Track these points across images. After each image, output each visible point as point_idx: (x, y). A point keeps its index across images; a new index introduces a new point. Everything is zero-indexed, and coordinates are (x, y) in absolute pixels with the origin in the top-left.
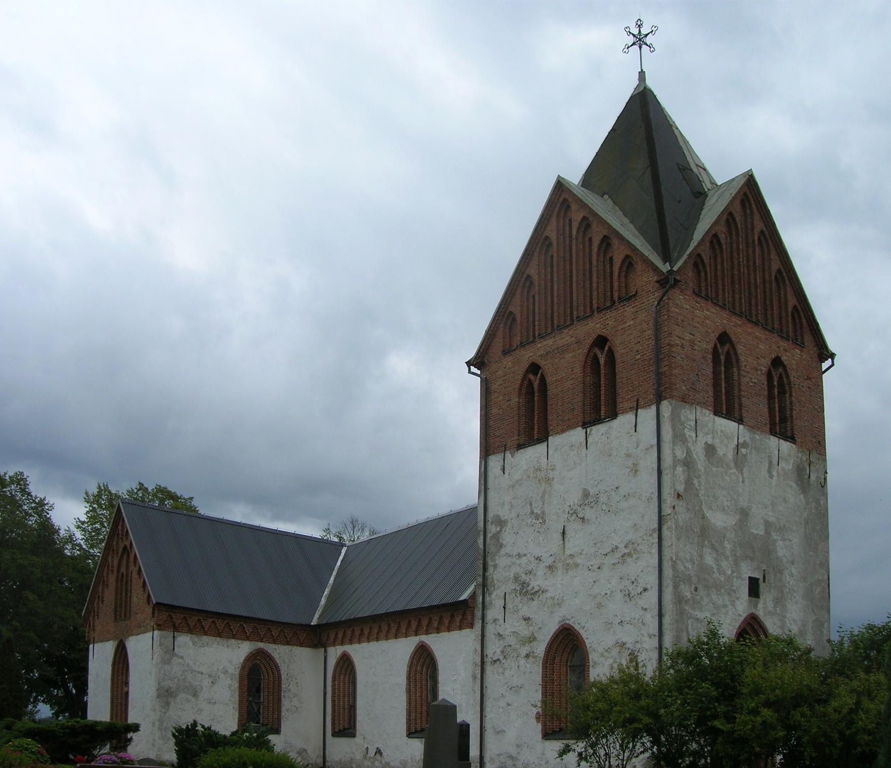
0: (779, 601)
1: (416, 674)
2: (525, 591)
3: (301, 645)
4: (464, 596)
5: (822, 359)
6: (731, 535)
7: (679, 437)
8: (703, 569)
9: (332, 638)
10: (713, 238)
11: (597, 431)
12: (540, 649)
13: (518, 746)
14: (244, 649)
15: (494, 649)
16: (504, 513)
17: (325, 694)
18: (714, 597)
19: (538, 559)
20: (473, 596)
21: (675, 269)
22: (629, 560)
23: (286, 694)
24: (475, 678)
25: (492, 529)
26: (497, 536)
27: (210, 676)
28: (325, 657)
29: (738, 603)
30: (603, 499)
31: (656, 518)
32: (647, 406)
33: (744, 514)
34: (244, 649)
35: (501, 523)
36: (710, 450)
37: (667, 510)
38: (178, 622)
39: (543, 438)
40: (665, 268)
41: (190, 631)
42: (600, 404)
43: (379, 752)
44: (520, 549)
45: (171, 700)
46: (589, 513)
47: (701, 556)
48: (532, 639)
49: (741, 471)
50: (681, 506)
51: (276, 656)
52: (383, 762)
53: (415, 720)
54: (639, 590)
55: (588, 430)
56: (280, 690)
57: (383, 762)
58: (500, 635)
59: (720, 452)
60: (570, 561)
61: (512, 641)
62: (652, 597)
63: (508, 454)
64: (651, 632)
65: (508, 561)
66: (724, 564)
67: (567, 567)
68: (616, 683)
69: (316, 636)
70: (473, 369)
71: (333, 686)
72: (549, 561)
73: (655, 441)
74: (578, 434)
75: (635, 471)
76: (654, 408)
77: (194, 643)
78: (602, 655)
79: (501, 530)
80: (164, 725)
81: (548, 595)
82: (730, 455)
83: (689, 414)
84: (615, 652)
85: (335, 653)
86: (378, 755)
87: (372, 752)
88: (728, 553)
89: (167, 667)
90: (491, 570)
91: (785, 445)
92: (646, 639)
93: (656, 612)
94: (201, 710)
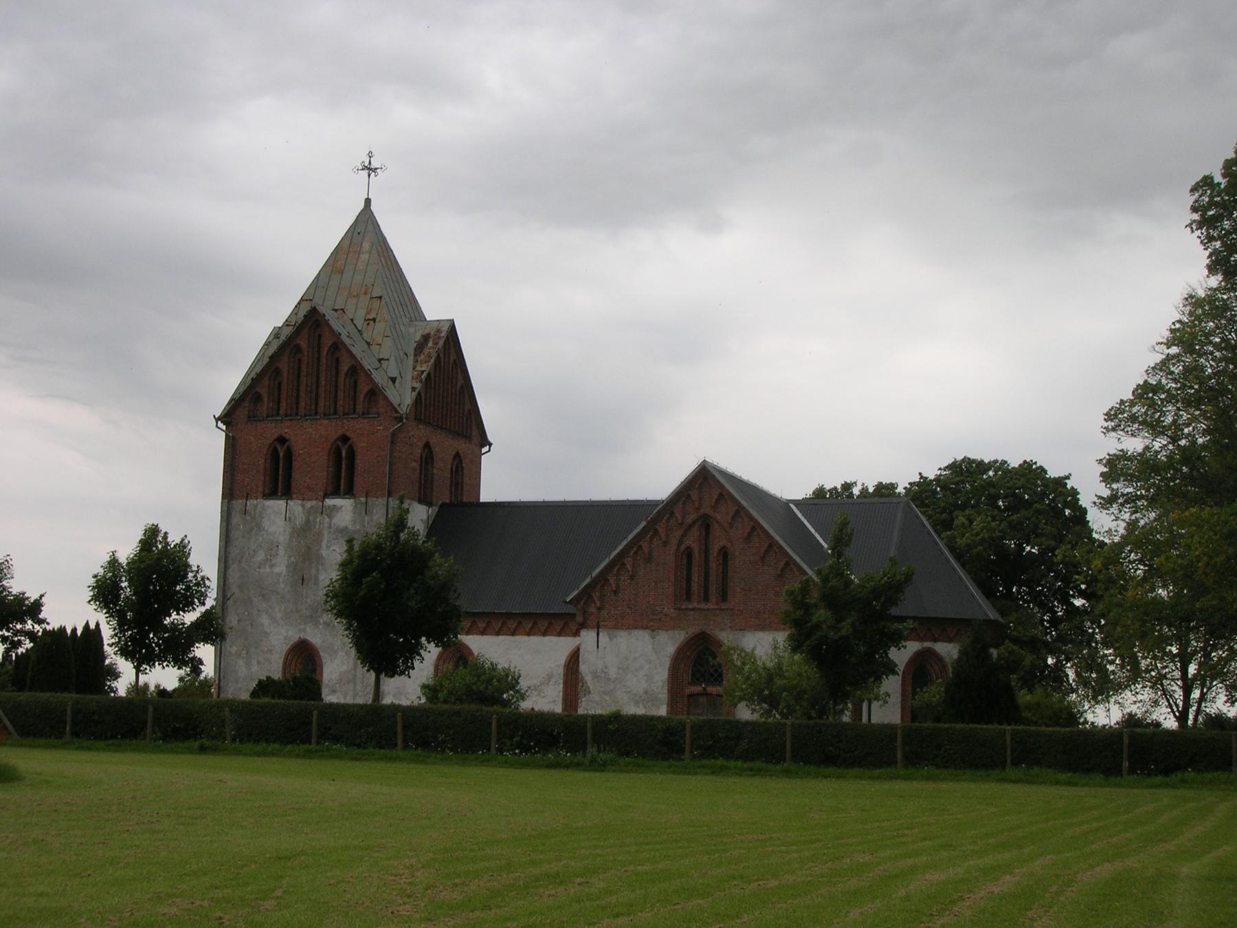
5: (483, 446)
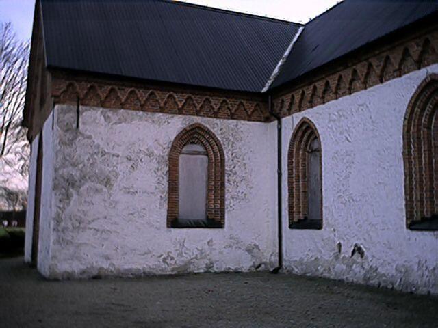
1: (419, 130)
3: (249, 118)
9: (287, 104)
14: (176, 124)
17: (280, 175)
23: (231, 178)
27: (129, 159)
28: (279, 131)
34: (176, 124)
38: (82, 94)
41: (102, 104)
43: (358, 250)
45: (72, 191)
51: (216, 132)
52: (366, 267)
53: (422, 201)
56: (223, 173)
57: (366, 267)
69: (267, 106)
71: (290, 164)
77: (106, 118)
80: (63, 224)
85: (290, 123)
86: (356, 254)
87: (347, 251)
89: (68, 150)
94: (116, 202)
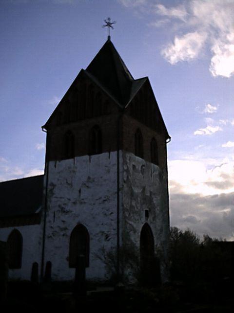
0: (154, 219)
2: (63, 211)
4: (37, 212)
6: (140, 195)
7: (125, 163)
8: (132, 207)
10: (136, 98)
11: (94, 157)
12: (69, 233)
13: (59, 270)
15: (49, 232)
16: (55, 182)
18: (135, 216)
19: (69, 200)
20: (41, 212)
21: (126, 107)
22: (106, 202)
24: (40, 243)
25: (50, 187)
26: (51, 190)
29: (142, 219)
30: (96, 180)
31: (116, 188)
32: (113, 150)
33: (144, 189)
35: (53, 185)
36: (134, 166)
37: (120, 186)
39: (72, 157)
40: (121, 106)
42: (95, 147)
44: (61, 196)
46: (90, 185)
47: (131, 202)
48: (66, 229)
49: (143, 174)
50: (125, 185)
51: (19, 230)
54: (110, 213)
55: (91, 156)
58: (52, 227)
59: (137, 168)
60: (82, 201)
61: (57, 229)
62: (115, 216)
63: (58, 162)
64: (115, 228)
65: (56, 199)
66: (138, 205)
67: (81, 203)
68: (176, 235)
70: (44, 129)
72: (73, 201)
73: (116, 163)
74: (86, 157)
75: (109, 172)
76: (116, 152)
78: (95, 236)
79: (54, 188)
81: (73, 213)
82: (140, 169)
83: (128, 155)
84: (100, 234)
88: (139, 201)
90: (48, 203)
91: (156, 166)
92: (112, 230)
93: (116, 221)
